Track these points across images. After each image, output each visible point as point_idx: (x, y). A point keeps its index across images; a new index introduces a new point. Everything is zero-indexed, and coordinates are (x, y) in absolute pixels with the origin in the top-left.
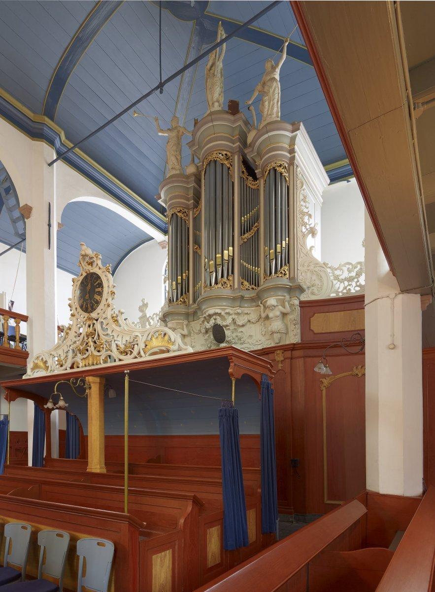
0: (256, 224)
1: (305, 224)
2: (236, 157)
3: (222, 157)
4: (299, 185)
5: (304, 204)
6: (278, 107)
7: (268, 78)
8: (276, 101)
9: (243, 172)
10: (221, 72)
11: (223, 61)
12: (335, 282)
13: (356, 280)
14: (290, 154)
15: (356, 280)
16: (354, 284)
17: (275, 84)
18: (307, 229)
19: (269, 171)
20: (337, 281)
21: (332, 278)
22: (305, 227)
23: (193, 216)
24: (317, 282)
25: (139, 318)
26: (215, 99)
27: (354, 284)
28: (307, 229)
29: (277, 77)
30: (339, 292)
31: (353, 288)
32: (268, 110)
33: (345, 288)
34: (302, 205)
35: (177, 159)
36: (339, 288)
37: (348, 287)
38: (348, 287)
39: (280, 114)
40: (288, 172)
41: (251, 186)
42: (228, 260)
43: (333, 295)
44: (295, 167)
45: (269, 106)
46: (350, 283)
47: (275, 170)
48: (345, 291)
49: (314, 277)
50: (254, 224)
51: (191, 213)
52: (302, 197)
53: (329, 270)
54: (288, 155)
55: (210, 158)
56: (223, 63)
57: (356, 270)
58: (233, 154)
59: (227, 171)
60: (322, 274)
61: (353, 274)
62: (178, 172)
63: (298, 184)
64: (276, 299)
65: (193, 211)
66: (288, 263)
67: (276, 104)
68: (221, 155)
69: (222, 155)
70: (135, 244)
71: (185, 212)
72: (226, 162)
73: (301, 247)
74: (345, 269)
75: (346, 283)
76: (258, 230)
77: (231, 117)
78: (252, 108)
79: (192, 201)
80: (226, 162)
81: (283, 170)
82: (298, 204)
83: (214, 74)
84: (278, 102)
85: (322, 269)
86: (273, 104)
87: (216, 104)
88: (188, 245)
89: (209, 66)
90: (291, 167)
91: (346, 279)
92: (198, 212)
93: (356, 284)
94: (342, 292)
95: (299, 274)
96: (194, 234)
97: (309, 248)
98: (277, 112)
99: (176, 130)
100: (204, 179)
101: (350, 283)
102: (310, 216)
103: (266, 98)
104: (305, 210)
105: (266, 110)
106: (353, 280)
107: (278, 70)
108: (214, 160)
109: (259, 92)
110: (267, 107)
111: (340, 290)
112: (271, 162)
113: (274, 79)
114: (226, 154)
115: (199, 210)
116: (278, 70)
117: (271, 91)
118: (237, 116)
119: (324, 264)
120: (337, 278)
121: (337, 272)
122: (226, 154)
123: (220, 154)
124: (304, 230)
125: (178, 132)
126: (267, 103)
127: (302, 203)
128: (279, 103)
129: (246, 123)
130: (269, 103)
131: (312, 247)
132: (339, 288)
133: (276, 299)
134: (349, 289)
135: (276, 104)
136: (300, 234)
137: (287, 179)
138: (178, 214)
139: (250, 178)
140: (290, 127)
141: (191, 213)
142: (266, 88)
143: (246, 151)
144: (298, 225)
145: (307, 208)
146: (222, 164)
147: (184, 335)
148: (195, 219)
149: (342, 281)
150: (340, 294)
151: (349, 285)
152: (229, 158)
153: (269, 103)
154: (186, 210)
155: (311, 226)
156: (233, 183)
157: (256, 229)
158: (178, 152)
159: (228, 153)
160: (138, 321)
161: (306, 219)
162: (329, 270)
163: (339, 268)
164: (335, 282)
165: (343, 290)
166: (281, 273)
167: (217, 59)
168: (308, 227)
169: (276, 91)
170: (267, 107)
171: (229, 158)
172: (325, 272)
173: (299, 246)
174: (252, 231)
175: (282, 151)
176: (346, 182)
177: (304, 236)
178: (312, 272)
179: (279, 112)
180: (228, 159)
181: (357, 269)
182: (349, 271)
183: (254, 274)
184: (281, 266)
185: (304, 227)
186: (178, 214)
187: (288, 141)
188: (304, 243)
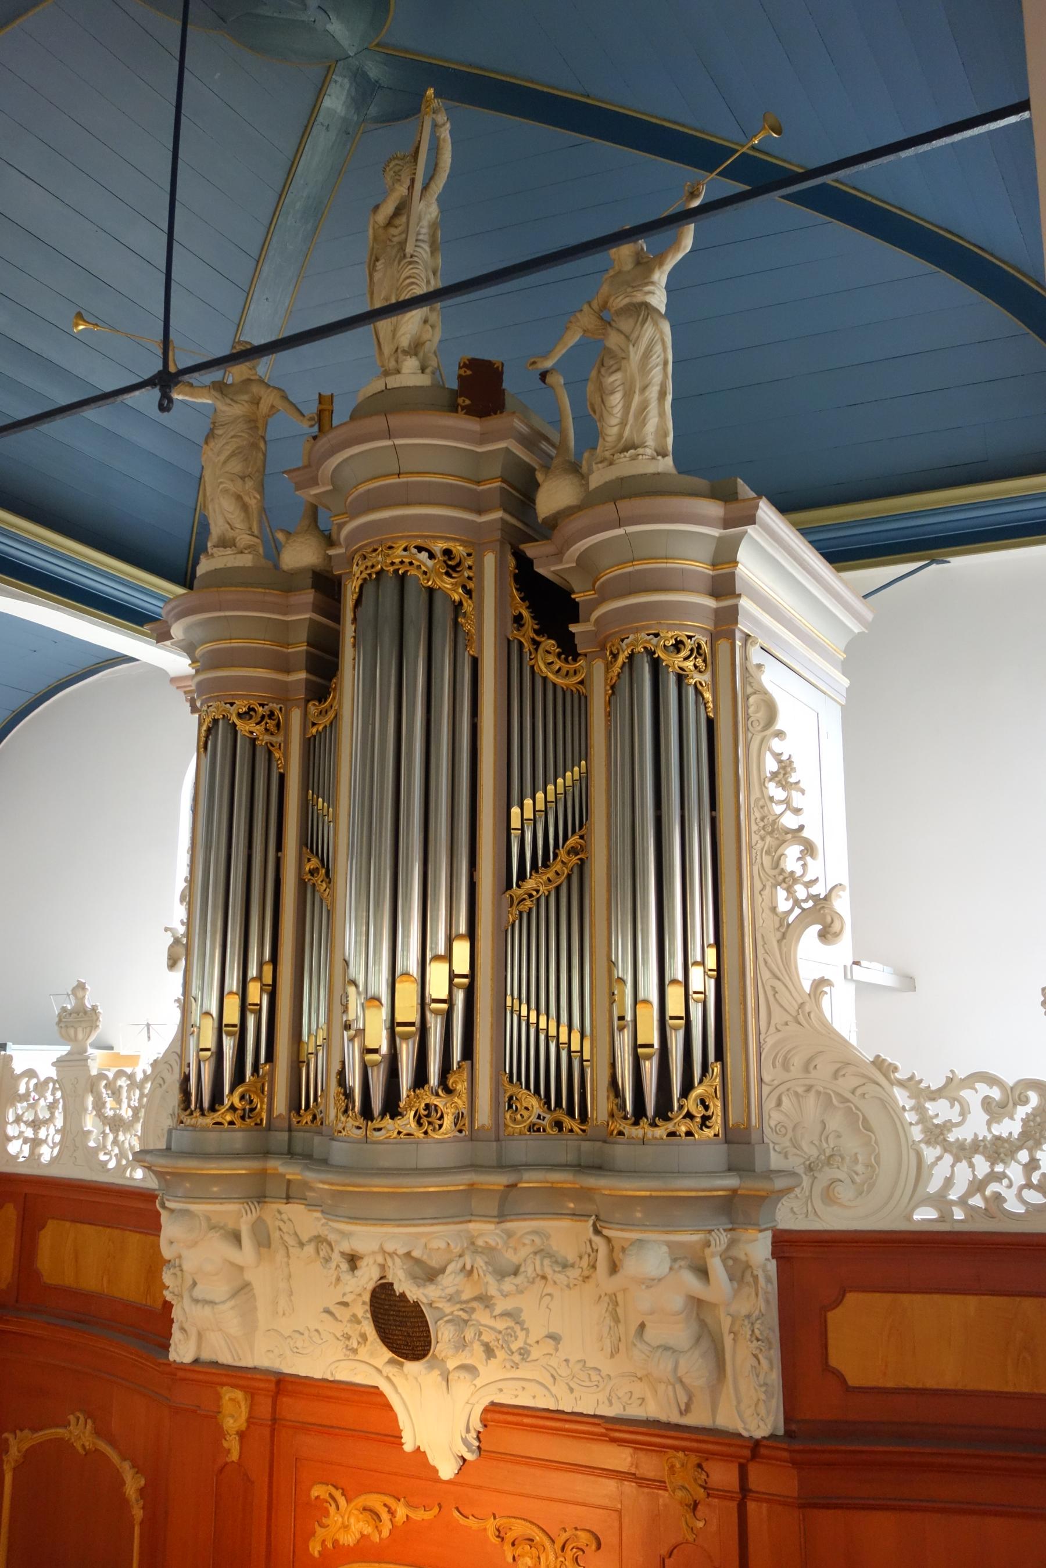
0: (573, 840)
1: (789, 881)
2: (490, 561)
3: (430, 563)
4: (758, 716)
5: (778, 793)
6: (662, 414)
7: (621, 302)
8: (653, 392)
9: (518, 619)
10: (433, 236)
11: (440, 200)
12: (930, 1153)
13: (1023, 1156)
14: (715, 594)
15: (1023, 1156)
16: (1015, 1172)
17: (649, 330)
18: (797, 903)
19: (631, 657)
20: (938, 1151)
21: (917, 1133)
22: (789, 890)
23: (304, 729)
24: (851, 1144)
25: (53, 1064)
26: (405, 342)
27: (1015, 1172)
28: (797, 903)
29: (659, 299)
30: (952, 1203)
31: (1014, 1190)
32: (623, 423)
33: (978, 1186)
34: (771, 799)
35: (245, 507)
36: (949, 1182)
37: (993, 1188)
38: (993, 1188)
39: (670, 440)
40: (711, 663)
41: (551, 676)
42: (450, 1001)
43: (924, 1215)
44: (738, 643)
45: (627, 408)
46: (999, 1168)
47: (656, 665)
48: (977, 1201)
49: (836, 1122)
50: (566, 839)
51: (296, 716)
52: (771, 765)
53: (901, 1096)
54: (711, 603)
55: (379, 561)
56: (439, 205)
57: (1022, 1112)
58: (476, 549)
59: (450, 616)
60: (877, 1119)
61: (1011, 1127)
62: (246, 560)
63: (751, 710)
64: (670, 1245)
65: (305, 714)
66: (720, 1056)
67: (653, 406)
68: (424, 556)
69: (432, 556)
70: (52, 681)
71: (271, 715)
72: (446, 584)
73: (778, 984)
74: (973, 1097)
75: (982, 1166)
76: (582, 865)
77: (472, 425)
78: (557, 380)
79: (302, 675)
80: (446, 584)
81: (689, 664)
82: (756, 793)
83: (402, 245)
84: (662, 394)
85: (870, 1088)
86: (644, 407)
87: (411, 364)
88: (279, 847)
89: (383, 216)
90: (723, 645)
91: (976, 1146)
92: (325, 720)
93: (1028, 1177)
94: (962, 1201)
95: (769, 1104)
96: (306, 807)
97: (807, 987)
98: (662, 434)
99: (246, 397)
100: (355, 620)
101: (999, 1168)
102: (809, 849)
103: (614, 379)
104: (789, 821)
105: (614, 421)
106: (1012, 1154)
107: (661, 277)
108: (396, 571)
109: (584, 331)
110: (618, 411)
111: (953, 1196)
112: (637, 630)
113: (643, 310)
114: (447, 552)
115: (331, 714)
116: (661, 277)
117: (635, 355)
118: (494, 422)
119: (878, 1063)
120: (936, 1134)
121: (941, 1110)
122: (447, 552)
123: (420, 549)
124: (784, 904)
125: (256, 402)
126: (616, 400)
127: (774, 790)
128: (669, 398)
129: (532, 440)
130: (628, 396)
131: (820, 984)
132: (949, 1182)
133: (670, 1245)
134: (998, 1197)
135: (653, 406)
136: (767, 924)
137: (708, 695)
138: (244, 727)
139: (550, 644)
140: (714, 509)
141: (296, 716)
142: (613, 340)
143: (530, 550)
144: (758, 886)
145: (797, 811)
146: (431, 591)
147: (258, 404)
148: (310, 746)
149: (963, 1151)
150: (959, 1214)
151: (999, 1177)
152: (459, 564)
153: (628, 396)
154: (275, 707)
155: (814, 890)
156: (475, 663)
157: (574, 860)
158: (249, 484)
159: (459, 550)
160: (53, 1073)
161: (791, 857)
162: (901, 1096)
163: (951, 1088)
164: (930, 1153)
165: (969, 1193)
166: (689, 1116)
167: (418, 186)
168: (801, 892)
169: (656, 359)
170: (618, 411)
171: (459, 564)
172: (887, 1105)
173: (766, 974)
174: (558, 867)
175: (682, 590)
176: (933, 1088)
177: (787, 932)
178: (827, 1101)
179: (666, 435)
180: (454, 568)
181: (1028, 1109)
182: (995, 1110)
183: (564, 1054)
184: (688, 1087)
185: (781, 893)
186: (244, 727)
187: (707, 552)
188: (788, 962)
